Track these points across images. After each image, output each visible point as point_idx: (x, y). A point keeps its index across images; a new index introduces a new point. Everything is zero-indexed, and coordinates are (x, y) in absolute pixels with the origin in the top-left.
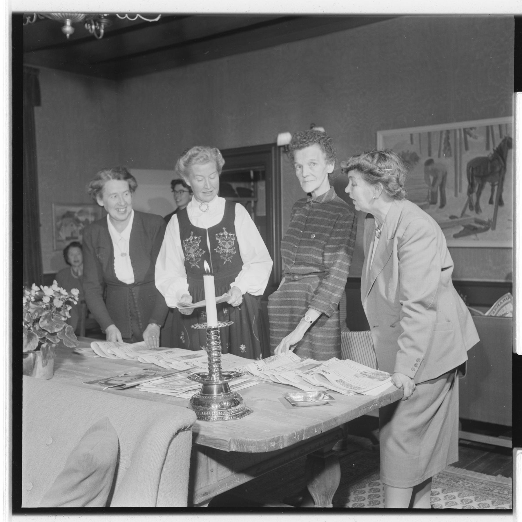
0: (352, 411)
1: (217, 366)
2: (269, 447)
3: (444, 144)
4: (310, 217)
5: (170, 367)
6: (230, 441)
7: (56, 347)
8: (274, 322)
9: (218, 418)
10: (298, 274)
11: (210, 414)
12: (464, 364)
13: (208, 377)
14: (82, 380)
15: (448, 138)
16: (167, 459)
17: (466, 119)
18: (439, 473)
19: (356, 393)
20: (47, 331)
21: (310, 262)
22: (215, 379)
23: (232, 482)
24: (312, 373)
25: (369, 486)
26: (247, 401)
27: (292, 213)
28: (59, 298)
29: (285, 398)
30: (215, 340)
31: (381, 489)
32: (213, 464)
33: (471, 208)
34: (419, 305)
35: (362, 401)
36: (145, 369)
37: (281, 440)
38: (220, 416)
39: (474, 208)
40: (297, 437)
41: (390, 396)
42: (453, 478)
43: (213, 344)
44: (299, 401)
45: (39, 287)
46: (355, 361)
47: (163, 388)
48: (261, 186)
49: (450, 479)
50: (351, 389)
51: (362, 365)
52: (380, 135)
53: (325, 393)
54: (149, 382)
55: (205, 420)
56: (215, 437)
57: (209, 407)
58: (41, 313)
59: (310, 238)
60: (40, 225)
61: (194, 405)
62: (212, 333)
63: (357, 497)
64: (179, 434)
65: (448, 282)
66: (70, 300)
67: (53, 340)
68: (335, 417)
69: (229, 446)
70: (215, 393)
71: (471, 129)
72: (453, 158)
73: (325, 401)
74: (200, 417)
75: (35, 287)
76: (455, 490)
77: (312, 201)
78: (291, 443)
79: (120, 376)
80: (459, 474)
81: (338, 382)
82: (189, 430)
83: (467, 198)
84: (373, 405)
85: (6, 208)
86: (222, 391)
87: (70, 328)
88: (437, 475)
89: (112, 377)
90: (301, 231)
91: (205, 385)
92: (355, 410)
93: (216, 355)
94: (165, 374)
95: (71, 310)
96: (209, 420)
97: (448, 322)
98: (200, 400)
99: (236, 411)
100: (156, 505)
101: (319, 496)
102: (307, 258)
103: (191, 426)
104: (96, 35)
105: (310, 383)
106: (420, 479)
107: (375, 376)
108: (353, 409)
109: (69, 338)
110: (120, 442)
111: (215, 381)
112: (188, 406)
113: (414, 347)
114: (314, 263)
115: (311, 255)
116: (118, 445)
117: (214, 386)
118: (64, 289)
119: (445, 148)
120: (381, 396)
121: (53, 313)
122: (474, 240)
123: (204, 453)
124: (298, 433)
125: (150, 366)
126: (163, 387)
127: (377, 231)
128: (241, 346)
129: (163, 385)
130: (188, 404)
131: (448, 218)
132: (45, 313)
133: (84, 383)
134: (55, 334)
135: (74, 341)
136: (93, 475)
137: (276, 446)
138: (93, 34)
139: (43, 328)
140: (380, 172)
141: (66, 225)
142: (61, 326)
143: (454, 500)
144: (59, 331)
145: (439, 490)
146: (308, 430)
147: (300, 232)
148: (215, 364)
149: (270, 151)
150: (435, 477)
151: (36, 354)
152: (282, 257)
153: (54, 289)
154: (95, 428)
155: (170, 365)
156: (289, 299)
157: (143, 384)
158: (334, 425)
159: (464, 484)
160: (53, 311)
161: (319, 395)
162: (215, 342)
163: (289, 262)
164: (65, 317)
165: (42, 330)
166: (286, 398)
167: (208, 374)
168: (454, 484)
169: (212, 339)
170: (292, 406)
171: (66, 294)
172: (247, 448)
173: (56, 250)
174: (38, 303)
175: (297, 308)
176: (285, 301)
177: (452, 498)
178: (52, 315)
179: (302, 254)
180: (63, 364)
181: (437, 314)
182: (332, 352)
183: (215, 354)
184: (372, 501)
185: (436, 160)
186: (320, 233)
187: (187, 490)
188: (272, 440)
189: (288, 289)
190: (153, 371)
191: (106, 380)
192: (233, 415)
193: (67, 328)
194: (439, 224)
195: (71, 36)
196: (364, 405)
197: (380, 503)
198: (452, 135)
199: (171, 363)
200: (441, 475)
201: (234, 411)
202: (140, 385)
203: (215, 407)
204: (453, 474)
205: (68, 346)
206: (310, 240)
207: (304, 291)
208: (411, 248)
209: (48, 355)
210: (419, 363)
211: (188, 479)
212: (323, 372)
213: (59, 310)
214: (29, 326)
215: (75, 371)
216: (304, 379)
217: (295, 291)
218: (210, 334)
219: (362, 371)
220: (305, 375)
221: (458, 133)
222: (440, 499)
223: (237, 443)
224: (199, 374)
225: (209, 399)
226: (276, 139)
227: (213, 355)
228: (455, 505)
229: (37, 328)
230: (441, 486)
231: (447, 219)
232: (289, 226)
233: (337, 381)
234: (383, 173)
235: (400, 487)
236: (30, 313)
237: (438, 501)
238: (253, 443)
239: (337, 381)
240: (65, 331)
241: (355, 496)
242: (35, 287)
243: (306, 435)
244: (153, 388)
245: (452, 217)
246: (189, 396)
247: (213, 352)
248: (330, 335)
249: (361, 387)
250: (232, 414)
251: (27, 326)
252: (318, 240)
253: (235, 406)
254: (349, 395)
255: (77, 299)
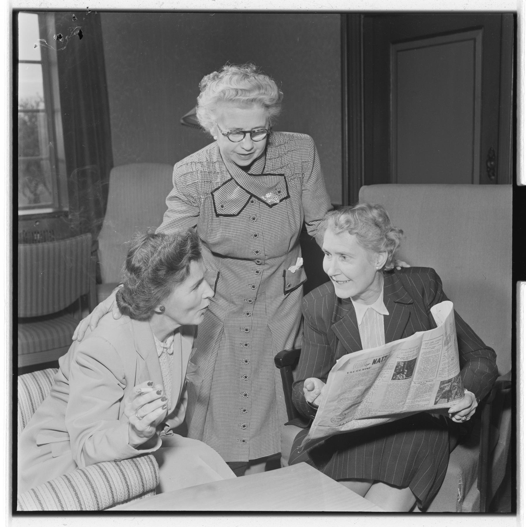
85: (7, 124)
128: (134, 265)
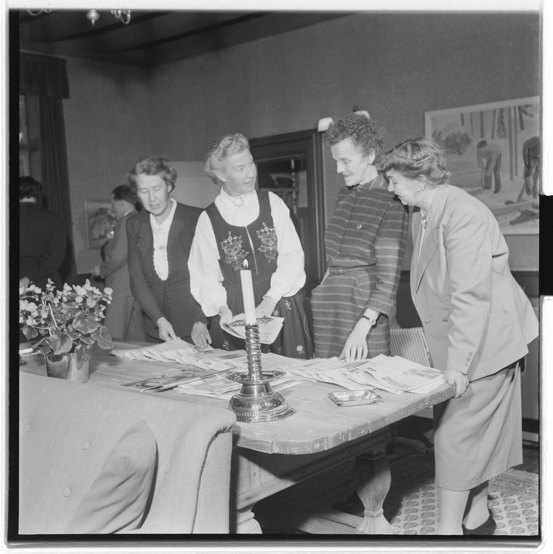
0: (400, 410)
1: (257, 365)
2: (313, 448)
3: (498, 123)
4: (356, 205)
5: (209, 368)
6: (272, 443)
7: (90, 349)
8: (318, 318)
9: (259, 419)
10: (343, 267)
11: (251, 415)
12: (524, 357)
13: (248, 376)
14: (119, 382)
15: (502, 117)
16: (206, 462)
17: (521, 96)
18: (498, 476)
19: (404, 391)
20: (81, 333)
21: (355, 255)
22: (255, 379)
23: (276, 486)
24: (357, 371)
25: (422, 490)
26: (289, 402)
27: (337, 199)
28: (92, 298)
29: (330, 398)
30: (254, 338)
31: (436, 493)
32: (256, 469)
33: (528, 192)
34: (469, 295)
35: (411, 400)
36: (183, 371)
37: (325, 441)
38: (262, 417)
39: (532, 192)
40: (342, 438)
41: (442, 394)
42: (512, 481)
43: (252, 342)
44: (345, 400)
45: (72, 287)
46: (407, 359)
47: (202, 389)
48: (303, 176)
49: (509, 481)
50: (398, 388)
51: (411, 362)
52: (428, 117)
53: (372, 392)
54: (188, 383)
55: (245, 421)
56: (256, 439)
57: (250, 408)
58: (74, 314)
59: (356, 229)
60: (73, 224)
61: (234, 406)
62: (251, 331)
63: (410, 502)
64: (219, 435)
65: (504, 271)
66: (104, 299)
67: (88, 342)
68: (382, 417)
69: (270, 447)
70: (256, 393)
71: (527, 106)
72: (507, 138)
73: (372, 401)
74: (240, 419)
75: (67, 287)
76: (515, 494)
77: (359, 188)
78: (337, 444)
79: (157, 378)
80: (519, 476)
81: (385, 380)
82: (229, 431)
83: (523, 181)
84: (423, 404)
86: (263, 391)
87: (104, 329)
88: (495, 477)
89: (149, 379)
90: (347, 221)
91: (245, 385)
92: (404, 409)
93: (256, 353)
94: (204, 375)
95: (105, 310)
96: (250, 421)
97: (505, 313)
98: (240, 401)
99: (278, 411)
100: (192, 531)
101: (368, 500)
102: (352, 250)
103: (230, 428)
104: (122, 21)
105: (355, 382)
106: (476, 482)
107: (425, 374)
108: (402, 408)
109: (104, 339)
110: (158, 445)
111: (255, 381)
112: (228, 408)
113: (466, 341)
114: (360, 255)
115: (357, 247)
116: (156, 448)
117: (254, 386)
118: (97, 288)
119: (499, 128)
120: (432, 393)
121: (86, 313)
122: (532, 226)
123: (246, 457)
124: (343, 433)
125: (187, 368)
126: (202, 388)
127: (422, 221)
129: (202, 386)
130: (227, 405)
131: (503, 204)
132: (79, 313)
133: (120, 385)
134: (89, 335)
135: (109, 342)
136: (130, 479)
137: (320, 447)
138: (120, 19)
139: (76, 330)
140: (418, 165)
141: (99, 223)
142: (95, 327)
143: (513, 504)
144: (94, 332)
145: (497, 494)
146: (354, 431)
147: (345, 222)
148: (255, 363)
149: (311, 138)
150: (494, 480)
151: (70, 357)
152: (326, 247)
153: (87, 289)
154: (132, 431)
155: (209, 366)
156: (333, 294)
157: (181, 386)
158: (382, 425)
159: (525, 487)
160: (86, 312)
161: (366, 394)
162: (254, 340)
163: (334, 254)
164: (99, 317)
165: (75, 331)
166: (331, 398)
167: (248, 374)
168: (514, 487)
169: (251, 337)
170: (337, 406)
171: (99, 293)
172: (290, 450)
173: (90, 249)
174: (71, 303)
175: (342, 303)
176: (328, 296)
177: (512, 501)
178: (86, 316)
179: (347, 246)
180: (99, 367)
181: (491, 304)
182: (380, 350)
183: (254, 353)
184: (426, 506)
185: (489, 141)
186: (367, 224)
187: (229, 494)
188: (316, 441)
189: (333, 283)
190: (192, 372)
191: (143, 383)
192: (275, 415)
193: (102, 329)
194: (493, 211)
195: (96, 22)
196: (413, 404)
197: (434, 508)
198: (506, 114)
199: (210, 364)
200: (500, 478)
201: (276, 412)
202: (178, 387)
203: (255, 408)
204: (513, 476)
205: (103, 348)
206: (356, 230)
207: (349, 286)
208: (456, 236)
209: (82, 357)
210: (472, 358)
211: (230, 483)
212: (369, 369)
213: (92, 310)
214: (62, 327)
215: (110, 374)
216: (349, 377)
217: (340, 286)
218: (249, 331)
219: (411, 368)
220: (350, 373)
221: (513, 111)
222: (499, 504)
223: (279, 445)
224: (238, 374)
225: (249, 400)
226: (317, 124)
227: (253, 353)
228: (515, 509)
229: (71, 330)
230: (500, 490)
231: (502, 205)
232: (334, 215)
233: (384, 379)
234: (421, 165)
235: (454, 490)
236: (62, 314)
237: (496, 505)
238: (296, 445)
239: (384, 379)
240: (99, 332)
241: (407, 501)
242: (67, 287)
243: (352, 436)
244: (192, 389)
245: (508, 203)
246: (229, 397)
247: (252, 350)
248: (378, 332)
249: (410, 385)
250: (274, 414)
251: (60, 327)
252: (365, 231)
253: (277, 406)
254: (397, 393)
255: (111, 298)
